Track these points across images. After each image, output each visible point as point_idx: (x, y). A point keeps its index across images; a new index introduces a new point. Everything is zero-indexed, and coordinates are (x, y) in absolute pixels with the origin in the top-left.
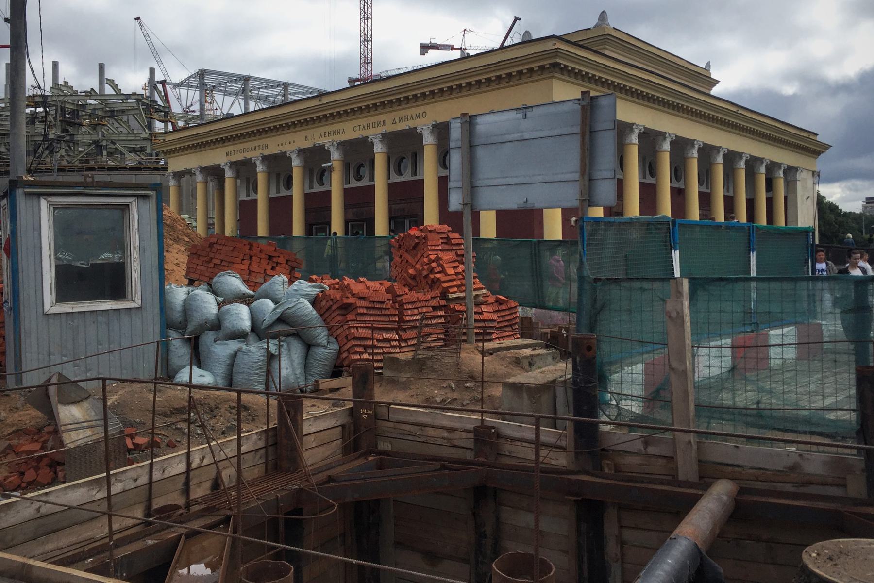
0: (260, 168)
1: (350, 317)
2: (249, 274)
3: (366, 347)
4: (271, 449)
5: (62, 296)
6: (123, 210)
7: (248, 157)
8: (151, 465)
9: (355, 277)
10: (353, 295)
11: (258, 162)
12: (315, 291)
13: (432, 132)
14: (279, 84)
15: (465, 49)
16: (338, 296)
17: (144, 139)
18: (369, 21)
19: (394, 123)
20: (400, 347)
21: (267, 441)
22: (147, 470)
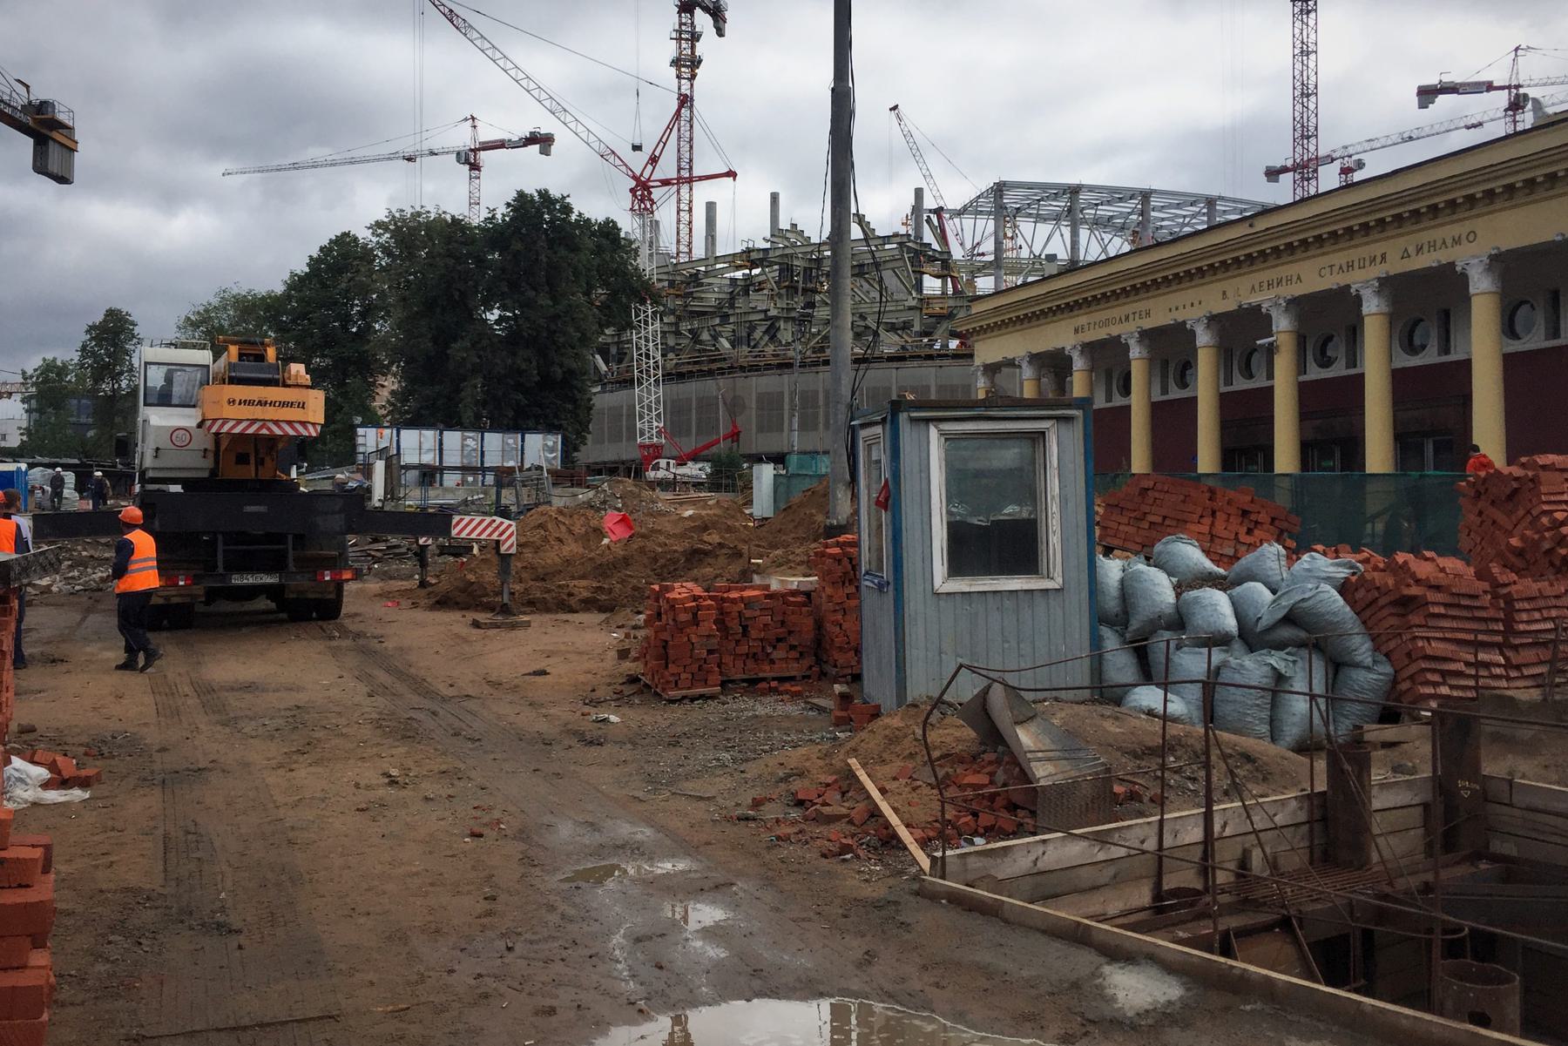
0: (1135, 352)
1: (1415, 619)
2: (1212, 540)
3: (1443, 673)
4: (1318, 827)
5: (957, 567)
6: (1033, 440)
7: (1115, 333)
8: (1161, 821)
9: (1415, 551)
10: (1418, 581)
11: (1132, 342)
12: (1343, 573)
13: (1489, 269)
14: (1131, 194)
15: (1518, 87)
16: (1391, 582)
17: (910, 308)
18: (1312, 57)
19: (1406, 255)
20: (1508, 678)
21: (1311, 812)
22: (1156, 828)
